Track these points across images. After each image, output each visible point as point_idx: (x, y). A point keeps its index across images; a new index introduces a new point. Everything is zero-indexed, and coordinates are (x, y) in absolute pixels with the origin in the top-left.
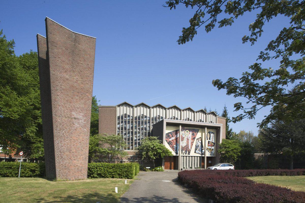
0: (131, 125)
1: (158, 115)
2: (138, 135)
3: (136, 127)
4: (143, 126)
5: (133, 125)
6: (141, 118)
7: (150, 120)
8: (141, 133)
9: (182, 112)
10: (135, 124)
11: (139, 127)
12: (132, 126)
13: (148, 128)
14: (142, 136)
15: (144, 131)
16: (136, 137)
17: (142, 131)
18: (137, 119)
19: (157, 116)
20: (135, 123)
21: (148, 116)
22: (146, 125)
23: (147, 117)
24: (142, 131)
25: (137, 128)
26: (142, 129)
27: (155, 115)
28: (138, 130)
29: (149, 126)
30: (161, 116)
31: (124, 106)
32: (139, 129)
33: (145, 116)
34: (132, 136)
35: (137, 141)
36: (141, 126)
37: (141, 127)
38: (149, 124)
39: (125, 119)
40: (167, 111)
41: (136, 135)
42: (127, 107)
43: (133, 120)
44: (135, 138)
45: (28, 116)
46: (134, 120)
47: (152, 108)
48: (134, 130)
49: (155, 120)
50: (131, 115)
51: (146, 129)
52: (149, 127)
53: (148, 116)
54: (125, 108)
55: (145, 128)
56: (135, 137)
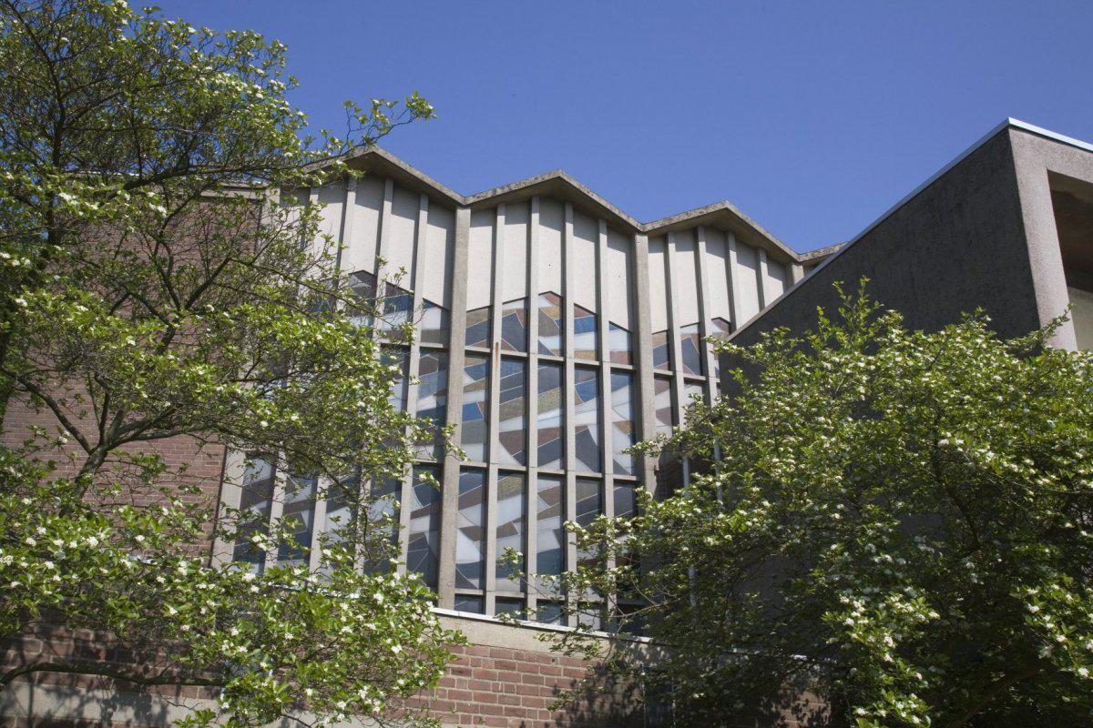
0: (422, 395)
1: (548, 295)
2: (502, 511)
3: (479, 418)
4: (564, 416)
5: (443, 393)
6: (541, 333)
7: (634, 355)
8: (535, 485)
9: (652, 263)
10: (467, 389)
11: (516, 424)
12: (430, 402)
13: (617, 445)
14: (555, 523)
15: (576, 467)
16: (479, 534)
17: (548, 469)
18: (498, 337)
19: (537, 304)
20: (470, 371)
21: (430, 287)
22: (593, 403)
23: (418, 303)
24: (554, 467)
25: (496, 428)
26: (555, 445)
27: (510, 288)
28: (502, 458)
29: (625, 413)
30: (387, 274)
31: (535, 217)
32: (517, 443)
33: (392, 288)
34: (424, 524)
35: (483, 586)
36: (541, 411)
37: (543, 419)
38: (624, 394)
39: (542, 348)
40: (640, 262)
41: (472, 516)
42: (388, 205)
43: (447, 342)
44: (461, 550)
45: (329, 332)
46: (649, 368)
47: (475, 222)
48: (466, 453)
49: (685, 362)
50: (615, 310)
51: (594, 452)
52: (635, 428)
53: (430, 287)
54: (545, 237)
55: (582, 433)
56: (468, 532)
